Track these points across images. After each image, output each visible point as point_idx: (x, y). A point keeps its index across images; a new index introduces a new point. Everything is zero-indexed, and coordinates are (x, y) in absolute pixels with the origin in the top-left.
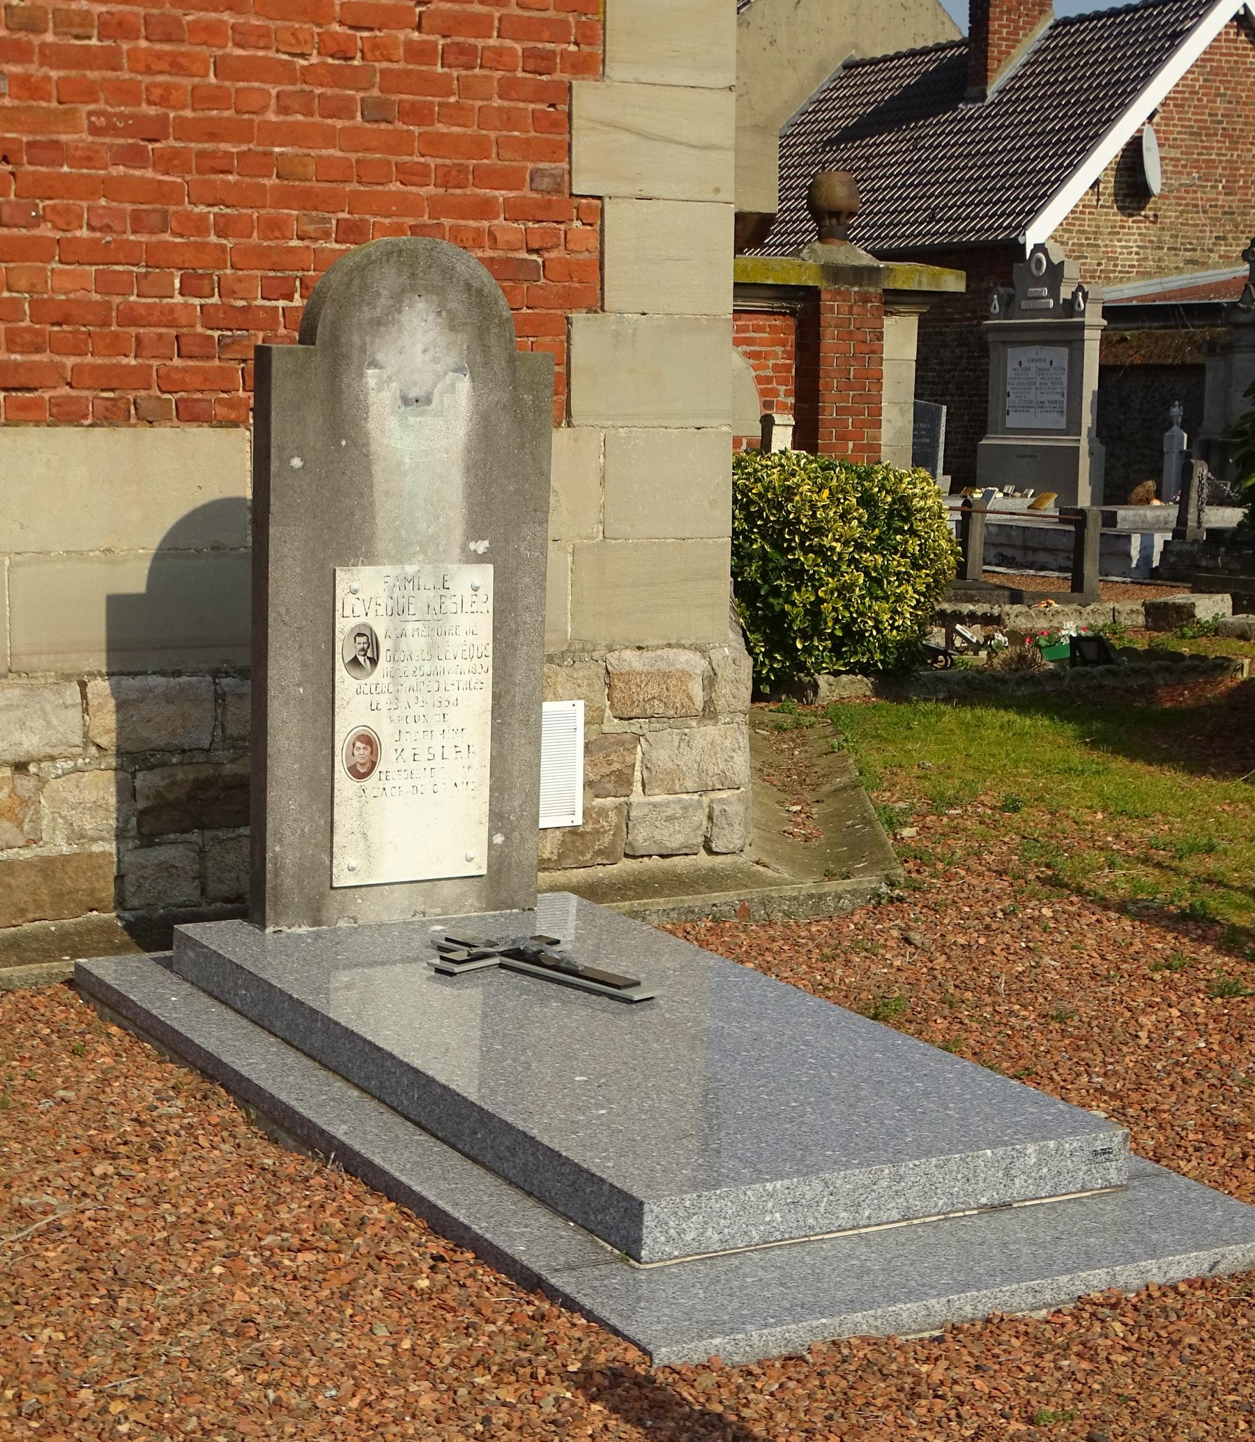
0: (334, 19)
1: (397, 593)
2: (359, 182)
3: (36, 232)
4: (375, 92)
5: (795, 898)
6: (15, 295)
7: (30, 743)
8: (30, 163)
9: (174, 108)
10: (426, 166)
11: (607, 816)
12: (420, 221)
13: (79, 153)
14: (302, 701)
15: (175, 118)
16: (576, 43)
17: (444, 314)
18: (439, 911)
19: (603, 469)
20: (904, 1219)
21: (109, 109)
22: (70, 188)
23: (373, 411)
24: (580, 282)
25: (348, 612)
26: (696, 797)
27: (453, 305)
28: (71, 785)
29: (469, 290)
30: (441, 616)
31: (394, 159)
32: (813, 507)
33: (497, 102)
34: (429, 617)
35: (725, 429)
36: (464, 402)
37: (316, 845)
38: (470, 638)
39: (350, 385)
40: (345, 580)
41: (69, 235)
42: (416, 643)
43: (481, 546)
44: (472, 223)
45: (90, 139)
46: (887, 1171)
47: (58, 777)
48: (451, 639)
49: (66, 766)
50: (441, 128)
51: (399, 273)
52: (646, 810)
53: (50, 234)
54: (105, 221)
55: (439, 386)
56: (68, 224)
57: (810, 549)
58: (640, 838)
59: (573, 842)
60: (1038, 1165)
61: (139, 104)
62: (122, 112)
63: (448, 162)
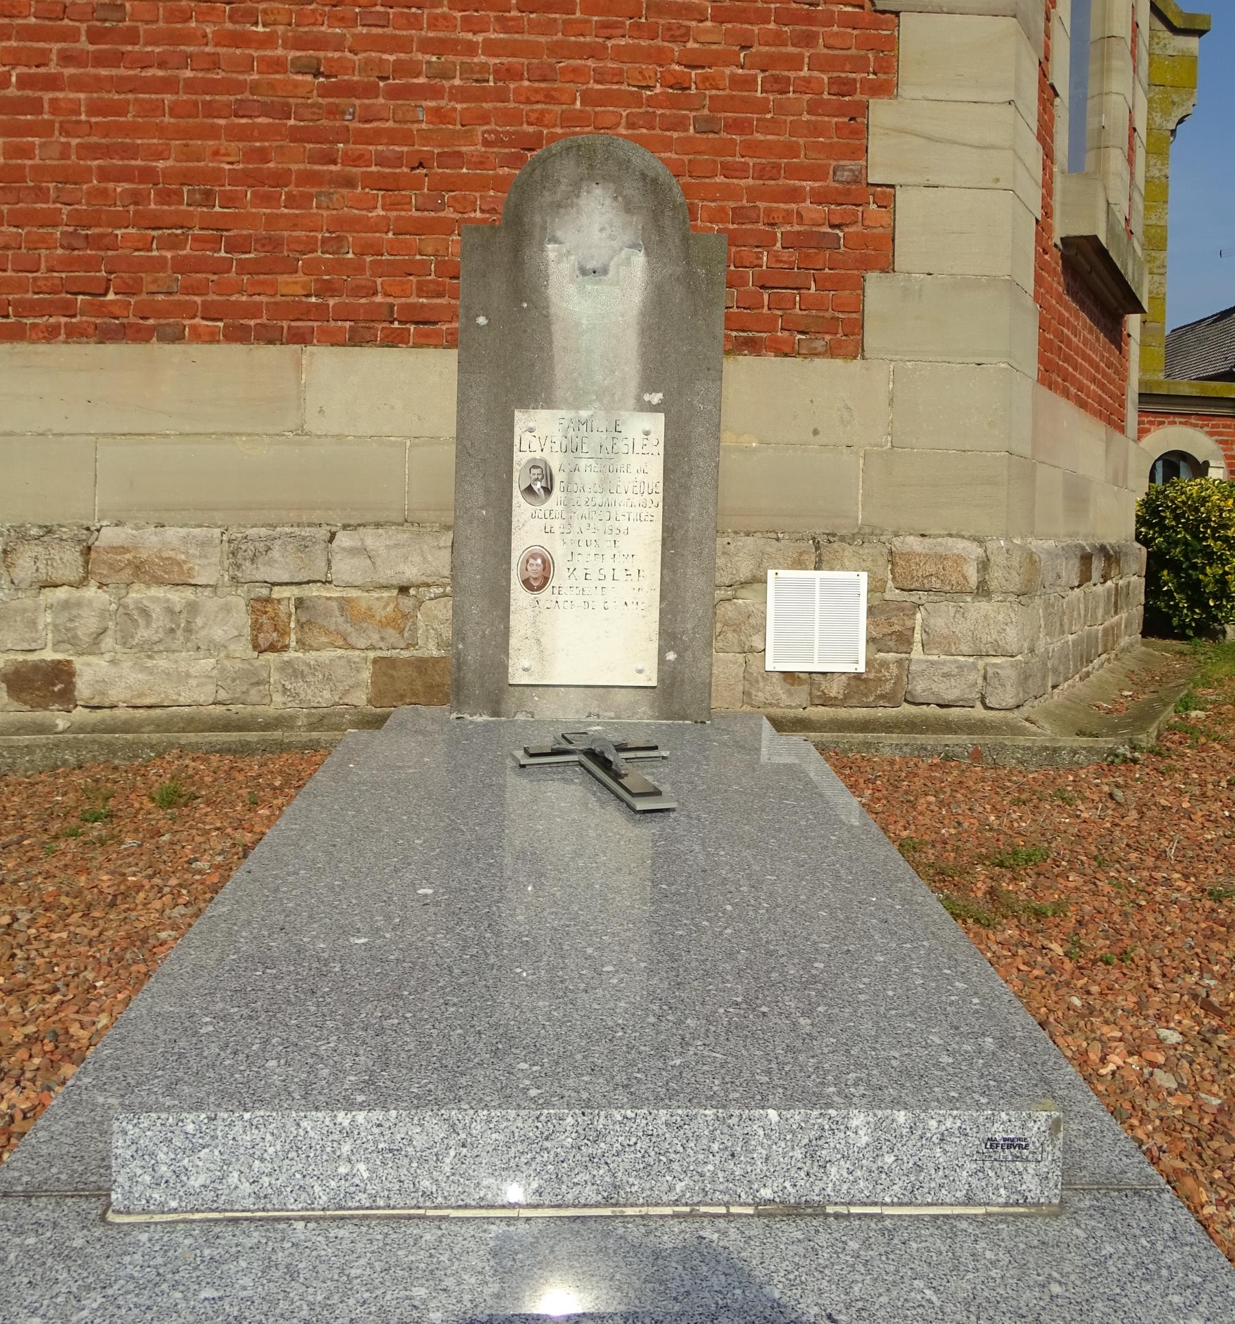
0: (673, 61)
1: (571, 433)
3: (442, 214)
4: (706, 112)
5: (1029, 748)
7: (411, 572)
9: (547, 126)
10: (746, 164)
11: (888, 668)
13: (474, 159)
14: (484, 521)
16: (875, 73)
18: (612, 714)
19: (892, 393)
20: (607, 1202)
23: (553, 279)
24: (875, 250)
26: (971, 659)
27: (629, 192)
29: (644, 179)
31: (719, 159)
32: (1221, 510)
33: (805, 117)
34: (601, 456)
35: (1002, 365)
38: (641, 476)
40: (522, 420)
41: (466, 216)
42: (588, 475)
43: (656, 398)
44: (782, 205)
46: (570, 1120)
47: (431, 599)
48: (624, 476)
50: (759, 136)
51: (578, 164)
52: (924, 666)
55: (615, 259)
57: (1219, 538)
58: (919, 689)
59: (858, 686)
60: (876, 1148)
61: (522, 124)
63: (764, 161)
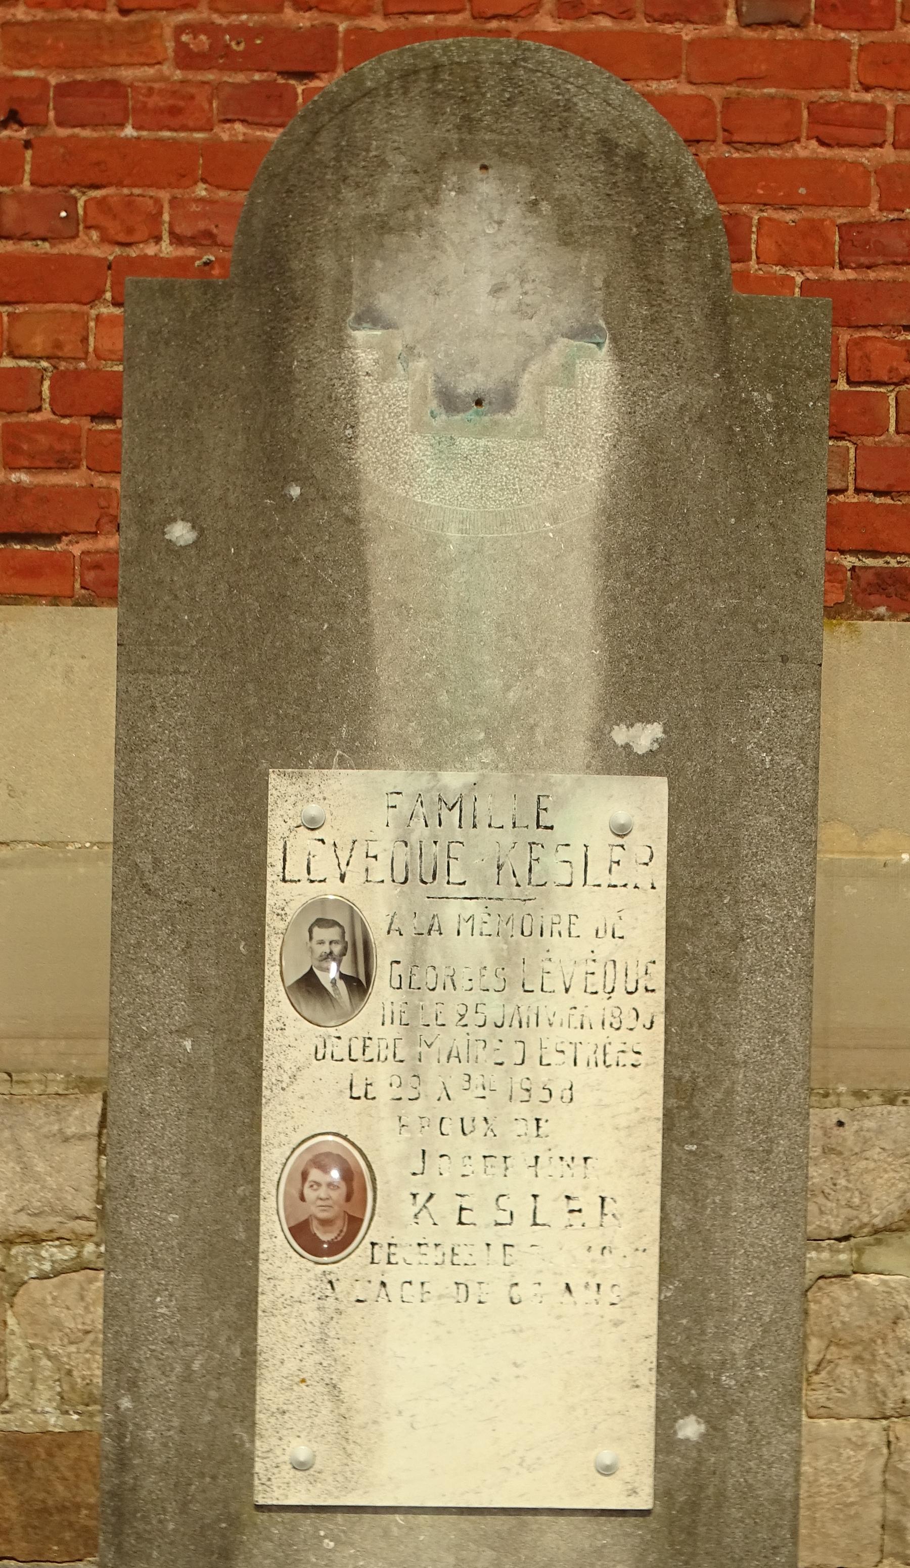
1: (419, 831)
2: (728, 143)
3: (70, 248)
6: (24, 363)
8: (60, 124)
9: (346, 13)
10: (876, 108)
12: (859, 215)
13: (154, 101)
15: (348, 32)
17: (545, 207)
21: (218, 19)
22: (135, 165)
23: (369, 421)
25: (295, 869)
27: (566, 189)
28: (70, 1294)
30: (530, 891)
34: (498, 892)
36: (598, 407)
37: (219, 1403)
39: (311, 365)
41: (133, 252)
43: (646, 737)
45: (178, 75)
47: (43, 1276)
49: (59, 1256)
53: (96, 252)
54: (202, 225)
55: (534, 367)
56: (130, 231)
62: (243, 25)
